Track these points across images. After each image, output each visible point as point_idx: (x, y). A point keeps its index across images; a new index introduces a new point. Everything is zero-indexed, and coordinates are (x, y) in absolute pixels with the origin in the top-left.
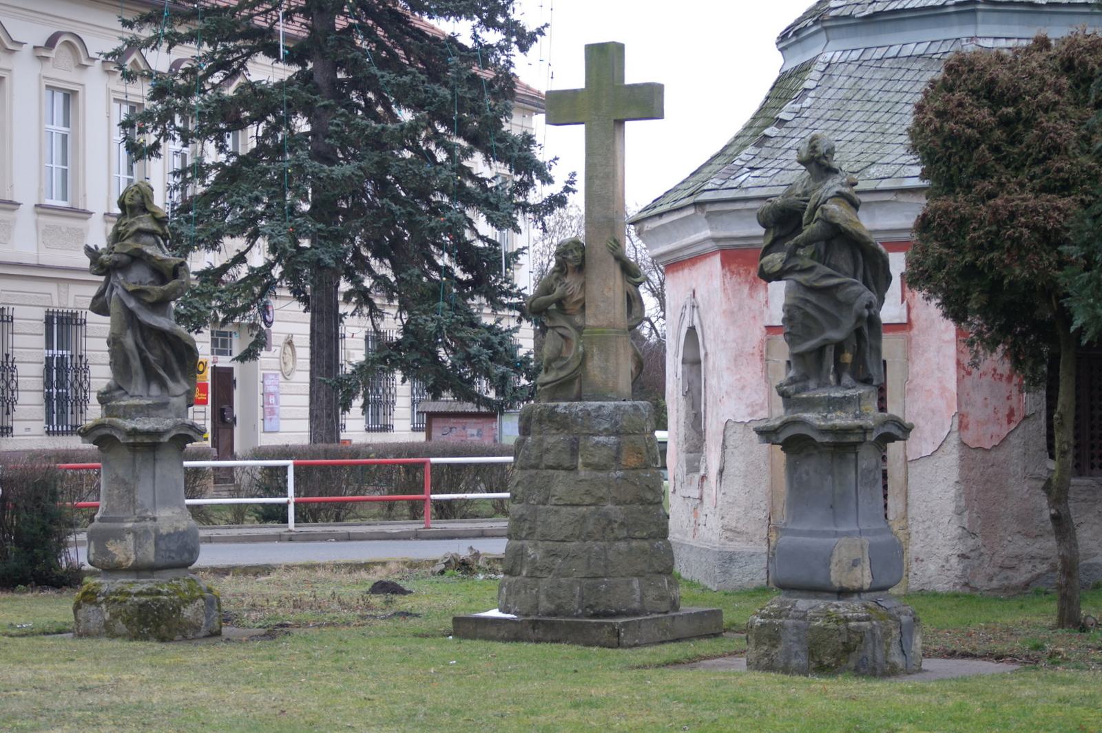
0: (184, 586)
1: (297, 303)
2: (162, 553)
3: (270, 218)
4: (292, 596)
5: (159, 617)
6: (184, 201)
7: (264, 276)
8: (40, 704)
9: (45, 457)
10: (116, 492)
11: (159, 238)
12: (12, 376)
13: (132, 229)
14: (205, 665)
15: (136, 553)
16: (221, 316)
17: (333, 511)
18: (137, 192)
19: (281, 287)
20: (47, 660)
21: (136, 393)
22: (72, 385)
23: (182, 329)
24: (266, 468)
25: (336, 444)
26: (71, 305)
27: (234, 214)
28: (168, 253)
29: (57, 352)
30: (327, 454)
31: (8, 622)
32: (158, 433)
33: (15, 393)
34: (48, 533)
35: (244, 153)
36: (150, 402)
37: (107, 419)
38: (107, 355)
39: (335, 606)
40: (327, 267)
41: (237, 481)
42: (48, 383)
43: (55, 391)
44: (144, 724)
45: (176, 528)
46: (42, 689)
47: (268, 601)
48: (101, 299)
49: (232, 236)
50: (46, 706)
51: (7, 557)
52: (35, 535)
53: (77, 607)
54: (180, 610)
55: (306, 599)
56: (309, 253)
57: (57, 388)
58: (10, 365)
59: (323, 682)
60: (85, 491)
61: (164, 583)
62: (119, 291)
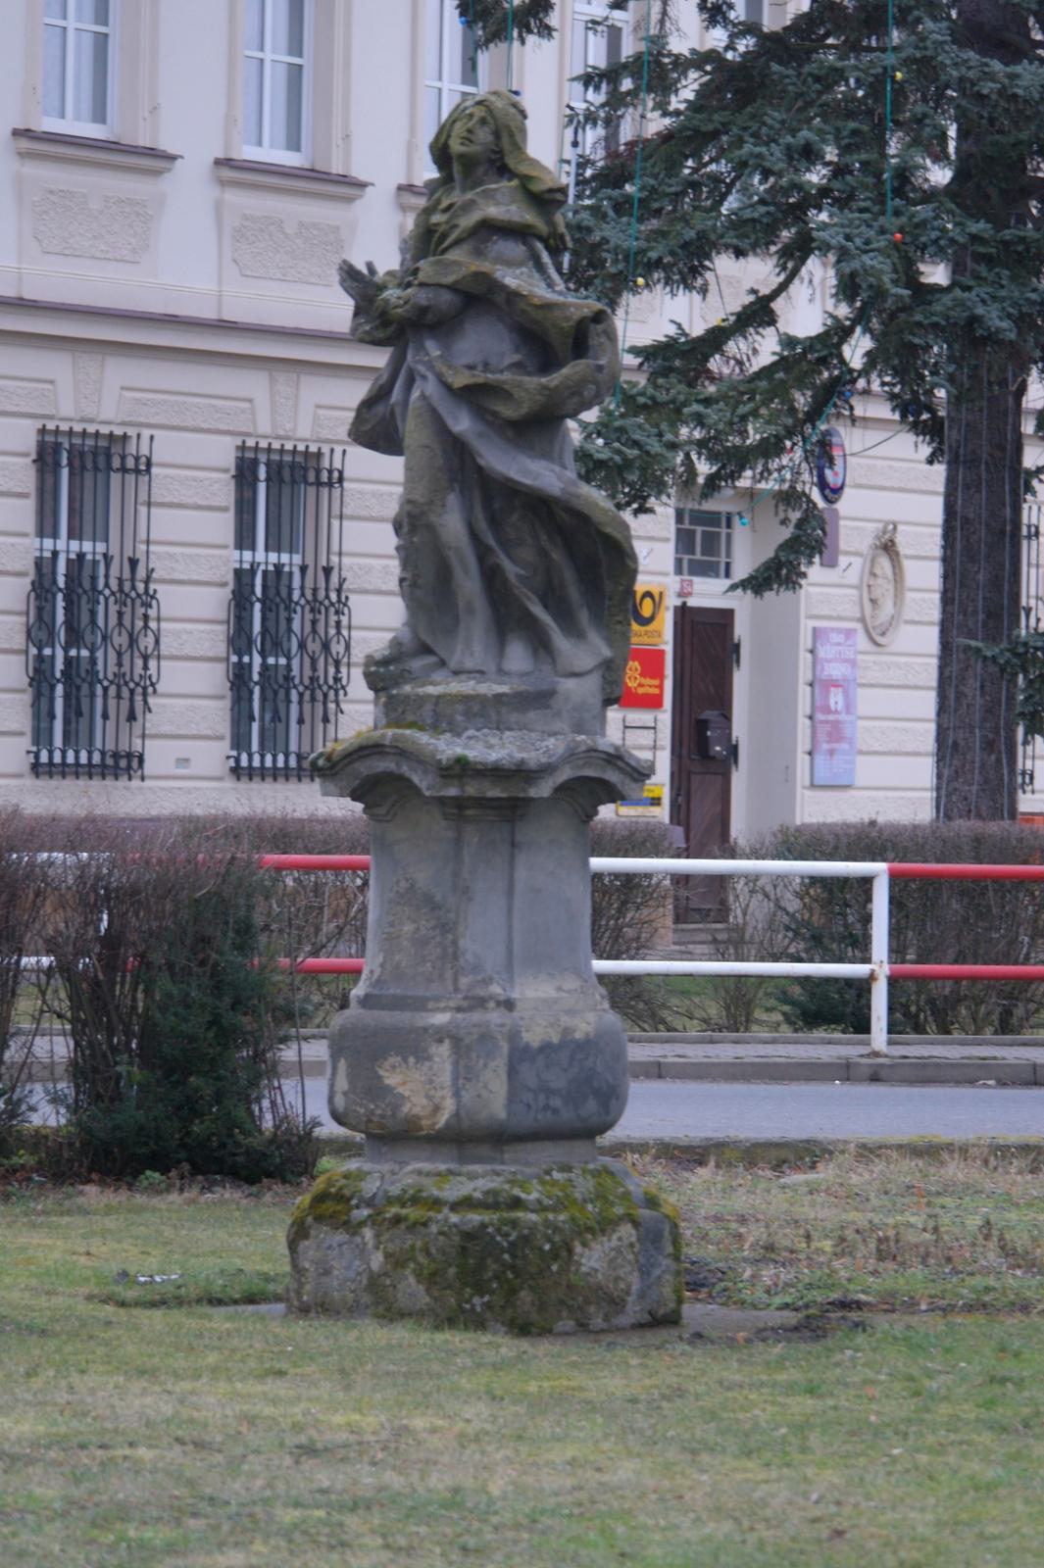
0: (584, 1186)
1: (911, 438)
2: (528, 1097)
3: (843, 203)
4: (874, 1227)
5: (513, 1268)
6: (612, 154)
7: (823, 361)
8: (191, 1483)
9: (225, 833)
10: (408, 928)
11: (539, 246)
12: (146, 617)
13: (467, 221)
14: (634, 1401)
15: (457, 1094)
16: (704, 468)
17: (994, 1004)
18: (483, 121)
19: (867, 392)
20: (214, 1370)
21: (469, 664)
22: (302, 645)
23: (595, 497)
24: (815, 880)
25: (1006, 823)
26: (304, 430)
27: (745, 190)
28: (561, 286)
29: (263, 557)
30: (980, 849)
31: (115, 1267)
32: (521, 774)
33: (152, 664)
34: (227, 1036)
35: (777, 27)
36: (504, 689)
37: (390, 732)
38: (394, 566)
39: (992, 1257)
40: (992, 338)
41: (736, 916)
42: (239, 639)
43: (257, 660)
44: (464, 1549)
45: (567, 1031)
46: (199, 1445)
47: (808, 1237)
48: (380, 409)
49: (739, 253)
50: (208, 1491)
51: (117, 1097)
52: (192, 1039)
53: (298, 1233)
54: (570, 1251)
55: (911, 1237)
56: (947, 299)
57: (263, 654)
58: (141, 587)
59: (952, 1459)
60: (328, 928)
61: (531, 1179)
62: (428, 387)
